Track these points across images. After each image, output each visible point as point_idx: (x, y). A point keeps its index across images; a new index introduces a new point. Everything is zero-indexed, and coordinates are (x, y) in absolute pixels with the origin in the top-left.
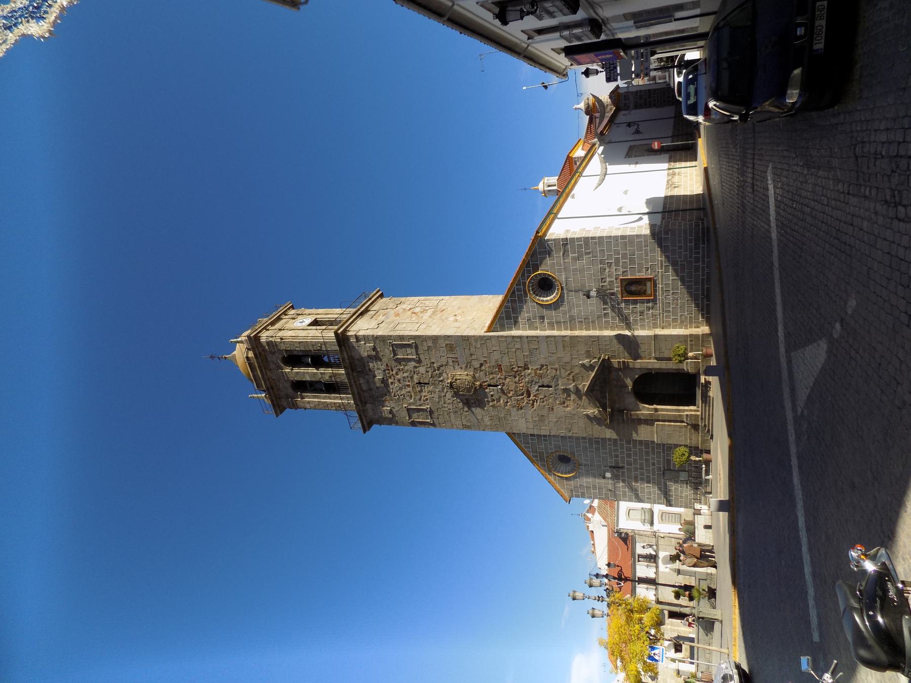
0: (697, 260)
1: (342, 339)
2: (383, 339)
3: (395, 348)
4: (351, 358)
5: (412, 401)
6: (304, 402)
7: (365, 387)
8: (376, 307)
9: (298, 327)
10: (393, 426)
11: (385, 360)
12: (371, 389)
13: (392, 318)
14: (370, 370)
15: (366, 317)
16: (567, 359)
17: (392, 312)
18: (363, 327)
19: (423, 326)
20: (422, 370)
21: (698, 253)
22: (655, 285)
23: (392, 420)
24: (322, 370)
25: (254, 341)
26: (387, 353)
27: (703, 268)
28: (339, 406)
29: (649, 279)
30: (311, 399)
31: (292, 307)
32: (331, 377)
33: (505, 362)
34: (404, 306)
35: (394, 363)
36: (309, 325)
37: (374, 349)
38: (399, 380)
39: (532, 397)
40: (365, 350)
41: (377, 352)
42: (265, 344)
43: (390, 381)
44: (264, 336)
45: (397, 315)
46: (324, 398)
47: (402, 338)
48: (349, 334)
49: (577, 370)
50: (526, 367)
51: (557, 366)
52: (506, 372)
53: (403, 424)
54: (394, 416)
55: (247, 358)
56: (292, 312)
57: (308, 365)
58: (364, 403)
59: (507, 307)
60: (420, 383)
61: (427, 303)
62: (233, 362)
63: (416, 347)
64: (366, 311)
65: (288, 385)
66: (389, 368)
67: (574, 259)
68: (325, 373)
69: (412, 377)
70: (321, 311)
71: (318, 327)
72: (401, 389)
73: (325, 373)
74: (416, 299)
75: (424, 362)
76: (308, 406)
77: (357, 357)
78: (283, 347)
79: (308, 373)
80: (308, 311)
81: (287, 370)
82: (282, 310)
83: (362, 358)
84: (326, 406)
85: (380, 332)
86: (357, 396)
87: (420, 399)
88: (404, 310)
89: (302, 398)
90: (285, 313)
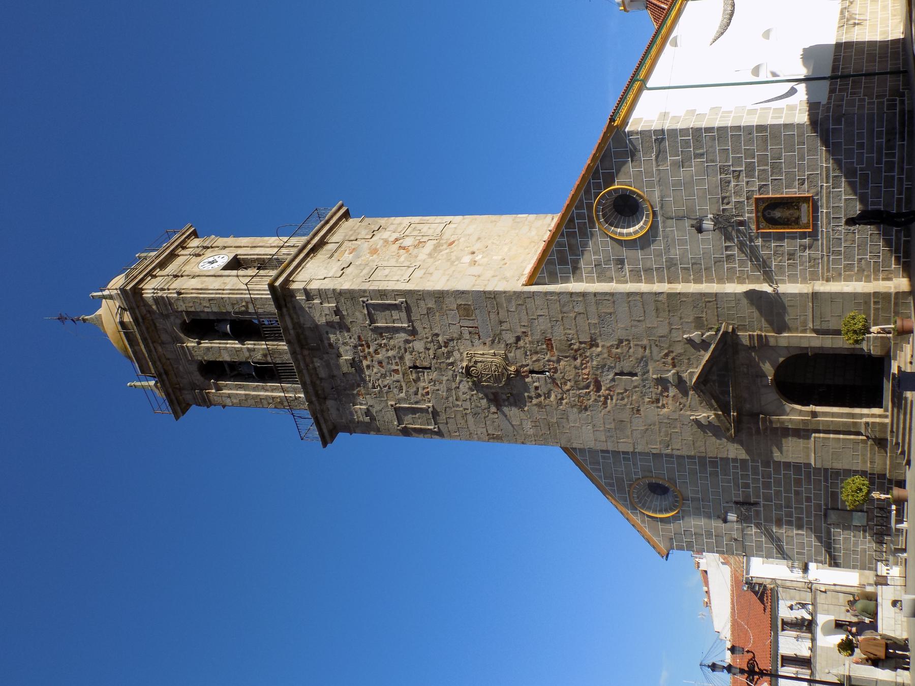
0: (890, 167)
1: (282, 295)
2: (351, 296)
3: (372, 311)
4: (298, 326)
5: (403, 395)
6: (221, 396)
7: (323, 373)
8: (337, 237)
9: (205, 272)
10: (372, 437)
11: (356, 330)
12: (333, 377)
13: (366, 257)
14: (330, 345)
15: (322, 255)
16: (663, 330)
18: (317, 274)
19: (418, 273)
20: (419, 346)
21: (893, 155)
22: (815, 209)
23: (370, 426)
24: (250, 344)
25: (132, 298)
26: (358, 317)
27: (900, 180)
28: (281, 403)
29: (806, 200)
30: (232, 390)
31: (195, 234)
32: (265, 356)
33: (558, 335)
34: (385, 235)
35: (370, 335)
36: (227, 267)
37: (337, 312)
38: (380, 363)
39: (603, 391)
40: (321, 313)
41: (342, 318)
42: (151, 302)
43: (365, 363)
44: (150, 288)
45: (374, 251)
47: (383, 294)
48: (294, 286)
49: (678, 349)
50: (593, 344)
51: (645, 342)
52: (560, 350)
53: (389, 432)
54: (373, 419)
55: (122, 323)
56: (195, 242)
57: (225, 336)
59: (560, 244)
60: (415, 367)
62: (97, 328)
63: (408, 310)
64: (322, 243)
65: (194, 368)
67: (674, 164)
68: (256, 349)
69: (402, 358)
70: (244, 241)
71: (241, 272)
72: (384, 376)
73: (256, 349)
76: (228, 402)
77: (308, 325)
78: (182, 307)
79: (227, 348)
80: (221, 241)
81: (191, 344)
82: (176, 239)
84: (259, 401)
85: (346, 285)
87: (416, 393)
88: (386, 241)
89: (219, 388)
90: (182, 246)
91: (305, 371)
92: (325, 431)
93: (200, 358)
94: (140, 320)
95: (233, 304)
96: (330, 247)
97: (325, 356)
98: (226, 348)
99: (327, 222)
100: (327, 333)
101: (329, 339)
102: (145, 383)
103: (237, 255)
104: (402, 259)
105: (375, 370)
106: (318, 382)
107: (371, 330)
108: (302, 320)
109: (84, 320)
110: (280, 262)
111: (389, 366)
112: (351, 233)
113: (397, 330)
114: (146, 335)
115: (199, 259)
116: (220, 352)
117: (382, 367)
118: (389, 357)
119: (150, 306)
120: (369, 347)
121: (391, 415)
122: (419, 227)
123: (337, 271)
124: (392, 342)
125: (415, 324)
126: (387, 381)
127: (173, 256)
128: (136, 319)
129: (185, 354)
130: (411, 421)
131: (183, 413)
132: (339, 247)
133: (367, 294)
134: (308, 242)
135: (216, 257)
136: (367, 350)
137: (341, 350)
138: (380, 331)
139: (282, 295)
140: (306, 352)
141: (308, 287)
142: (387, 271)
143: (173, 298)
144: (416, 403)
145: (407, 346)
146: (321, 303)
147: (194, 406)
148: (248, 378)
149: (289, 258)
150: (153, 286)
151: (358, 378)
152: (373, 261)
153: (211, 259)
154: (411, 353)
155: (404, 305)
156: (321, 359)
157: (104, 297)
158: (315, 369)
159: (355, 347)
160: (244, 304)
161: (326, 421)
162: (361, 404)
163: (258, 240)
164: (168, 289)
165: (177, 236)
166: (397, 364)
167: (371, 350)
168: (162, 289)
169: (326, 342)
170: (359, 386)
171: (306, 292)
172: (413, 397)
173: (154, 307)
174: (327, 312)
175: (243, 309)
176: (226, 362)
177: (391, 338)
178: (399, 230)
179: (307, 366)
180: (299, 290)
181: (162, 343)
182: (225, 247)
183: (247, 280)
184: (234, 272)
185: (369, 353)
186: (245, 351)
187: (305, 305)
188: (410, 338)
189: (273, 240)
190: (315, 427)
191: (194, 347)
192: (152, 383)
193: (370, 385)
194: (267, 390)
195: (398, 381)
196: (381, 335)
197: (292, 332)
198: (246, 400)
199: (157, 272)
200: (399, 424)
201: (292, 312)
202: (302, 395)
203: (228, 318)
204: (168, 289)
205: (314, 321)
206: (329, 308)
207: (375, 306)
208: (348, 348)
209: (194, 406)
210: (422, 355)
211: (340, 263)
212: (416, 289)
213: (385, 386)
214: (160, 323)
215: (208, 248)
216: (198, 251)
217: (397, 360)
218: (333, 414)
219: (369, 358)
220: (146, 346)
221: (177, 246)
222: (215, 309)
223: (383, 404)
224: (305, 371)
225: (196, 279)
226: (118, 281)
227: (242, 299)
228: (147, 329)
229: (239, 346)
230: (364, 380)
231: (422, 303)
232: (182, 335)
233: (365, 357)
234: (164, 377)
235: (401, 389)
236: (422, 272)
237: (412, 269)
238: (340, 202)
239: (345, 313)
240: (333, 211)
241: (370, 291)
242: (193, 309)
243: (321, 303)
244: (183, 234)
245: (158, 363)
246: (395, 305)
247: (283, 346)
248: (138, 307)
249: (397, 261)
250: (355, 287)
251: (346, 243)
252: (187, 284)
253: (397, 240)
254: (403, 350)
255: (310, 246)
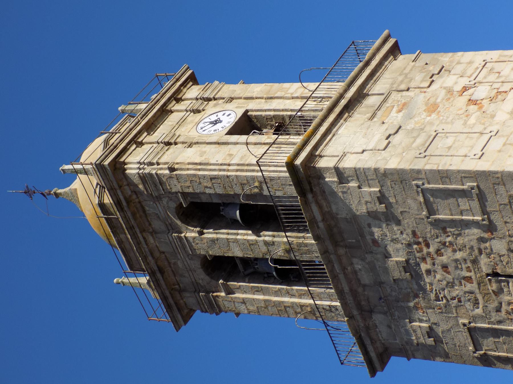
1: (305, 176)
2: (401, 178)
3: (430, 200)
4: (329, 217)
5: (479, 311)
6: (233, 301)
7: (366, 278)
8: (380, 86)
9: (203, 140)
10: (438, 364)
11: (408, 222)
12: (381, 284)
13: (422, 117)
14: (375, 242)
15: (360, 114)
17: (420, 99)
18: (354, 147)
19: (496, 144)
20: (499, 246)
23: (434, 349)
24: (267, 236)
25: (112, 173)
26: (412, 207)
28: (312, 312)
30: (248, 294)
31: (193, 80)
32: (288, 251)
34: (448, 81)
35: (429, 231)
36: (232, 132)
37: (382, 198)
38: (445, 267)
40: (360, 200)
41: (389, 206)
42: (136, 180)
43: (424, 267)
44: (135, 161)
45: (432, 108)
46: (277, 293)
47: (444, 175)
48: (322, 163)
53: (462, 360)
54: (438, 341)
55: (102, 205)
56: (193, 92)
57: (233, 224)
58: (366, 312)
60: (495, 274)
61: (506, 69)
62: (71, 205)
63: (482, 198)
64: (360, 96)
65: (196, 264)
66: (416, 240)
68: (274, 242)
69: (475, 262)
70: (257, 89)
71: (252, 138)
72: (451, 285)
73: (274, 242)
74: (478, 57)
75: (502, 229)
76: (242, 308)
77: (343, 215)
78: (176, 187)
79: (238, 240)
80: (228, 90)
81: (191, 233)
82: (169, 87)
83: (354, 219)
84: (283, 310)
85: (392, 162)
86: (350, 299)
87: (498, 310)
88: (450, 91)
89: (230, 291)
90: (176, 98)
91: (341, 276)
92: (373, 355)
93: (203, 252)
94: (124, 204)
95: (242, 185)
96: (371, 101)
97: (369, 257)
98: (236, 241)
99: (367, 64)
100: (369, 226)
101: (372, 234)
102: (133, 280)
103: (247, 111)
104: (472, 120)
105: (438, 277)
106: (360, 290)
107: (431, 223)
108: (334, 208)
109: (57, 195)
110: (306, 122)
111: (458, 272)
112: (400, 78)
113: (468, 224)
114: (133, 222)
115: (198, 116)
116: (229, 245)
117: (448, 273)
118: (456, 261)
119: (136, 186)
120: (428, 246)
121: (463, 338)
122: (498, 67)
123: (380, 140)
124: (460, 241)
125: (492, 217)
126: (457, 291)
127: (164, 112)
128: (118, 203)
129: (184, 247)
130: (493, 347)
131: (186, 322)
132: (385, 101)
133: (423, 176)
134: (341, 96)
135: (220, 115)
136: (425, 250)
137: (390, 249)
138: (444, 225)
139: (305, 176)
140: (341, 251)
141: (341, 166)
142: (449, 141)
143: (164, 175)
144: (500, 322)
145: (483, 246)
146: (359, 187)
147: (198, 312)
148: (266, 277)
149: (320, 114)
150: (138, 159)
151: (416, 287)
152: (431, 123)
153: (213, 118)
154: (488, 255)
155: (475, 191)
156: (363, 259)
157: (76, 172)
158: (355, 272)
159: (409, 245)
160: (257, 184)
161: (373, 342)
162: (421, 321)
163: (275, 88)
164: (158, 164)
165: (168, 84)
166: (468, 270)
167: (432, 250)
168: (151, 164)
169: (368, 237)
170: (416, 296)
171: (338, 171)
172: (493, 314)
173: (141, 187)
174: (368, 199)
175: (256, 190)
176: (237, 257)
177: (459, 235)
178: (469, 73)
179: (344, 269)
180: (327, 169)
181: (154, 233)
182: (231, 99)
183: (260, 150)
184: (243, 138)
185: (429, 254)
186: (261, 244)
187: (338, 189)
188: (486, 235)
189: (294, 88)
190: (356, 348)
191: (194, 238)
192: (144, 280)
193: (433, 296)
194: (293, 296)
195: (471, 293)
196: (444, 230)
197: (321, 225)
198: (266, 307)
199: (144, 137)
200: (476, 350)
201: (320, 198)
202: (338, 304)
203: (237, 201)
204: (158, 164)
205: (351, 210)
206: (370, 193)
207: (435, 193)
208: (399, 246)
209: (198, 312)
210: (505, 259)
211: (385, 126)
212: (493, 168)
213: (453, 299)
214: (150, 207)
215: (209, 100)
216: (197, 105)
217: (469, 264)
218: (383, 333)
219: (428, 260)
220: (134, 236)
221: (169, 99)
222: (220, 191)
223: (452, 323)
224: (341, 276)
225: (195, 148)
226: (93, 152)
227: (253, 178)
228: (134, 214)
229: (253, 238)
230: (424, 290)
231: (501, 189)
232: (179, 223)
233: (424, 259)
234: (158, 276)
235: (476, 303)
236: (502, 140)
237: (486, 137)
238: (386, 32)
239: (392, 200)
240: (376, 46)
241: (426, 172)
242: (191, 190)
243: (359, 187)
244: (178, 80)
245: (150, 258)
246: (463, 191)
247: (309, 239)
248: (120, 187)
249: (465, 124)
250: (405, 166)
251: (395, 96)
252: (182, 156)
253: (465, 89)
254: (476, 251)
255: (343, 102)
